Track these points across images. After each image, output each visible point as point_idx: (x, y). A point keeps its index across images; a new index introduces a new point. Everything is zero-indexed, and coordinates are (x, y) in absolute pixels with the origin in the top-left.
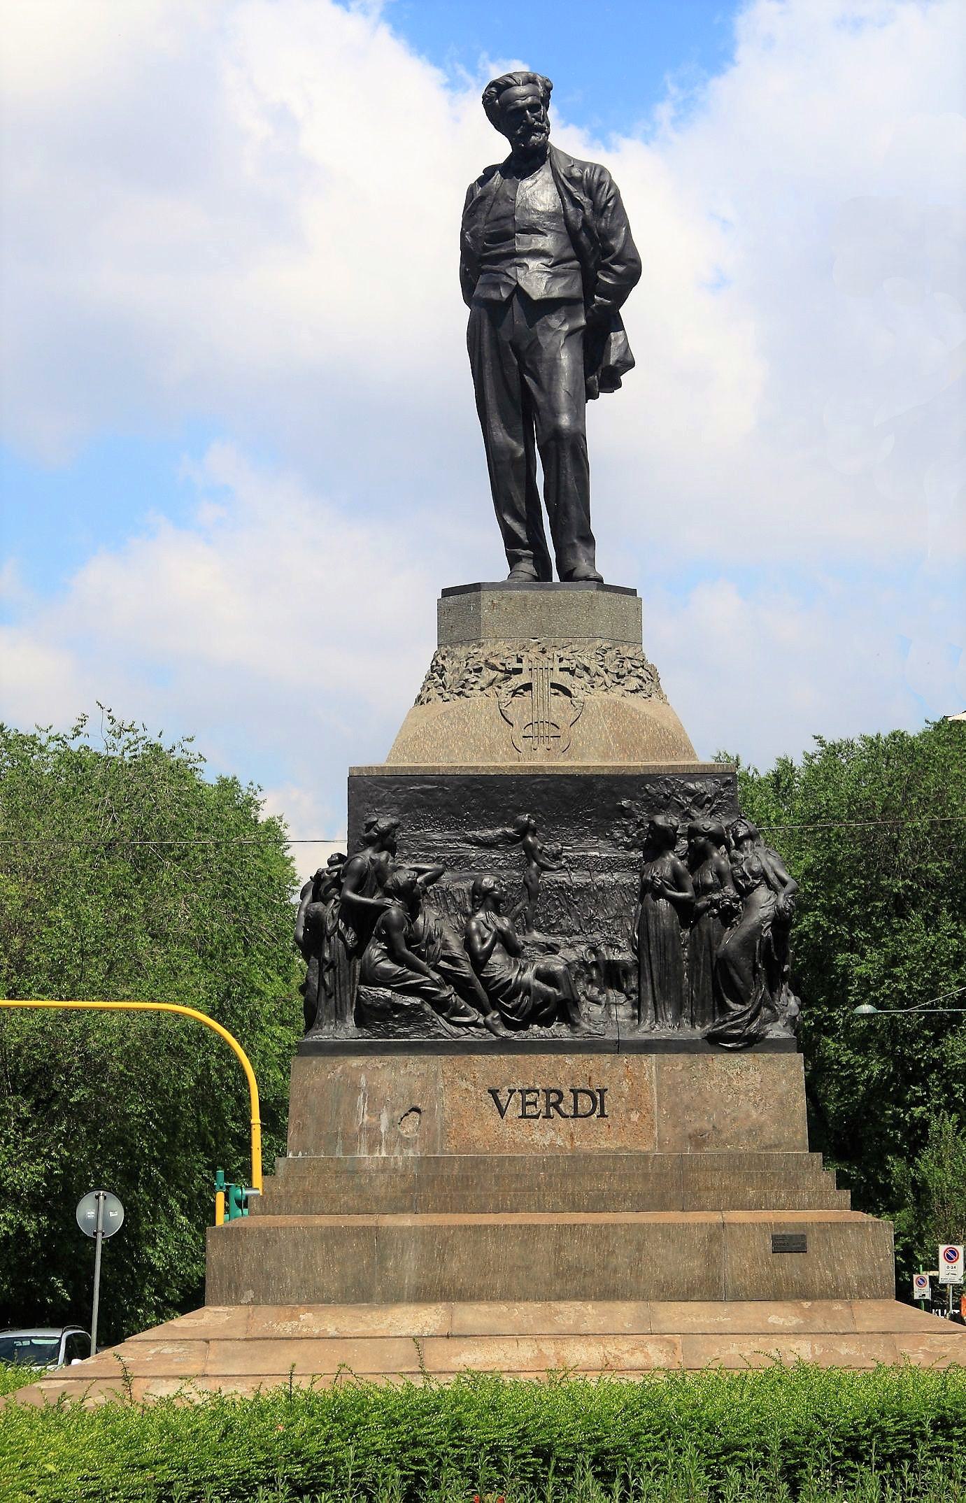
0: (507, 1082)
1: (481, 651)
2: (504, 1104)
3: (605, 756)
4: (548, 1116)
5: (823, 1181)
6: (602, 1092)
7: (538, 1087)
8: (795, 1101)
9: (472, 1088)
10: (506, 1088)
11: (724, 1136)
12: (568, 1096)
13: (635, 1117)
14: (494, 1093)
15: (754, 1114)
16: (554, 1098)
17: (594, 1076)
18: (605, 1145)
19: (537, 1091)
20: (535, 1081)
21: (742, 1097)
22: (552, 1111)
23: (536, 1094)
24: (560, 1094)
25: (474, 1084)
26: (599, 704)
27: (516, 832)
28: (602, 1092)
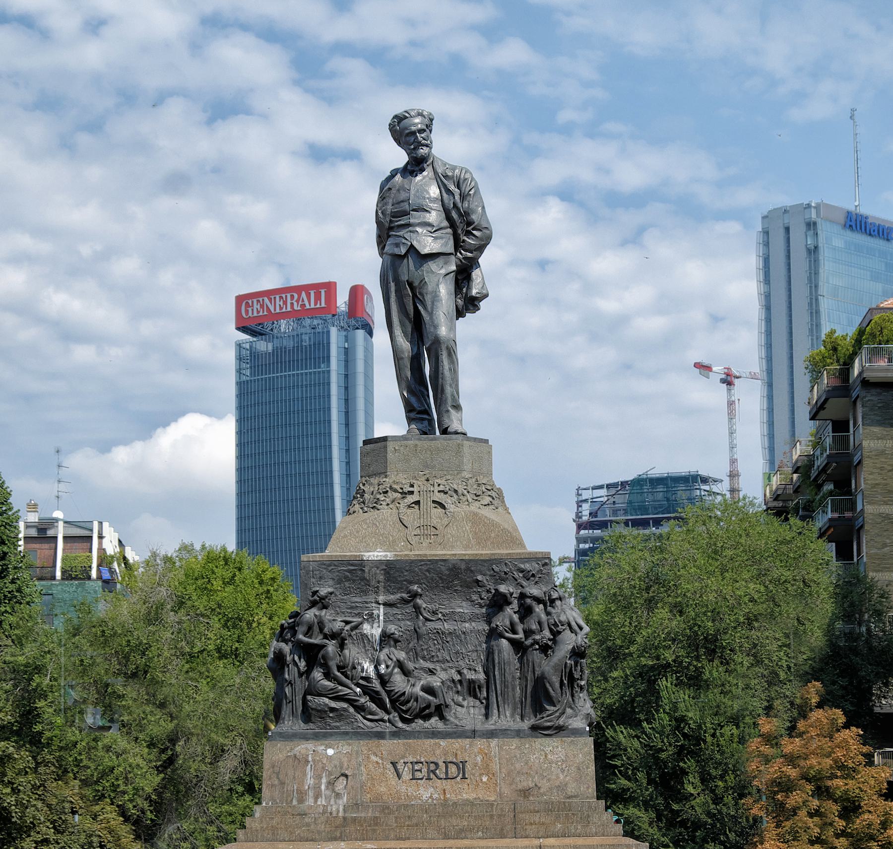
0: (403, 757)
1: (387, 480)
2: (401, 771)
3: (467, 547)
4: (429, 779)
5: (605, 818)
6: (464, 763)
7: (422, 760)
8: (587, 768)
9: (380, 762)
10: (402, 761)
11: (542, 791)
12: (442, 766)
13: (485, 779)
14: (394, 764)
15: (562, 777)
16: (432, 767)
17: (459, 753)
18: (465, 796)
19: (421, 763)
20: (420, 756)
21: (554, 765)
22: (432, 776)
23: (421, 765)
24: (436, 764)
25: (382, 758)
26: (463, 513)
27: (409, 597)
28: (464, 763)
